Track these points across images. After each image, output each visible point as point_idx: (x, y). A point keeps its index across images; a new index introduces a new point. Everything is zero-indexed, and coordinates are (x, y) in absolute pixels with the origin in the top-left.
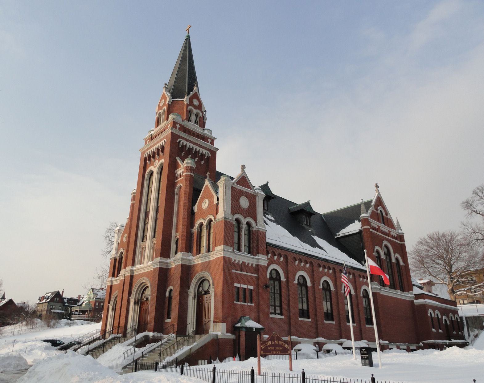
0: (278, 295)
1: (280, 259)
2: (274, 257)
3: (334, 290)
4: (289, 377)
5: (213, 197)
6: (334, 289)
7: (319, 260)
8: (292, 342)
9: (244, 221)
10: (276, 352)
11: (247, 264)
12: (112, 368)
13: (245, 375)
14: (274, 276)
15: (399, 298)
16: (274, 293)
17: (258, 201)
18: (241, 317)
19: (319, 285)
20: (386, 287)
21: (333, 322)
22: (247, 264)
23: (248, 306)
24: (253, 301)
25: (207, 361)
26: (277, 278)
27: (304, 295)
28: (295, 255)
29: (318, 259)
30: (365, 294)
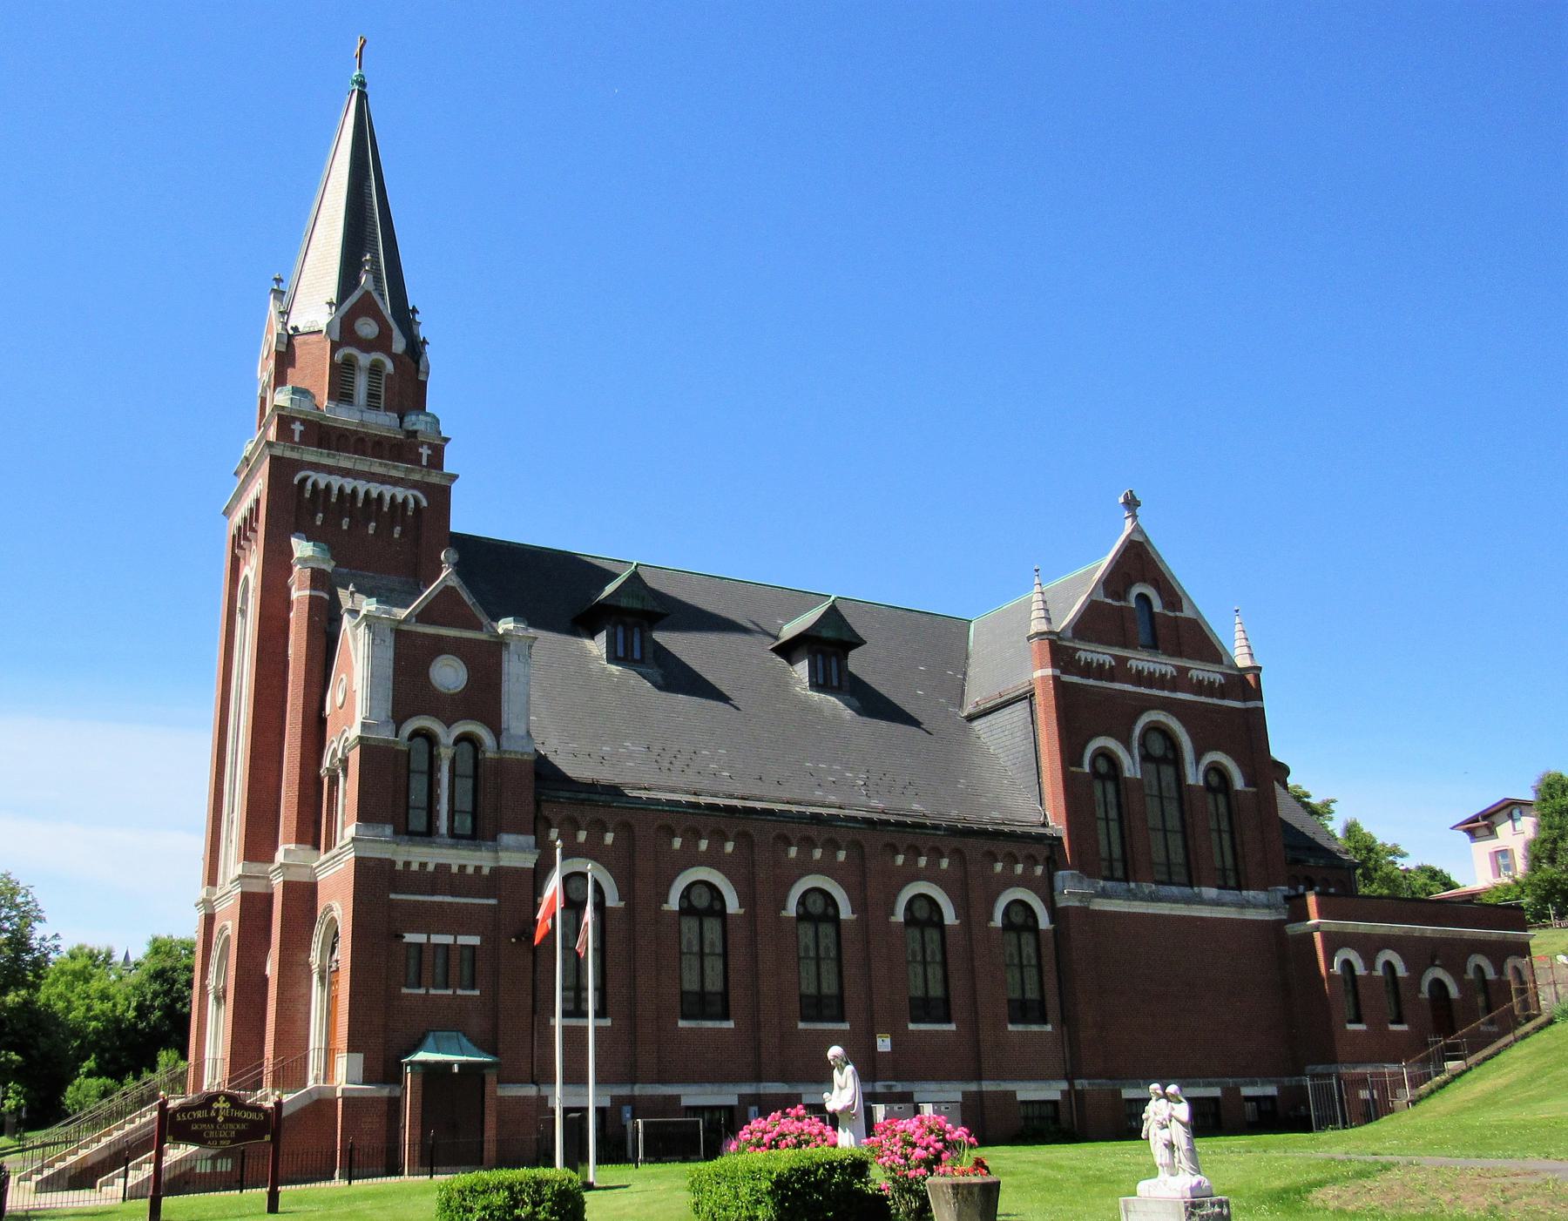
0: (1034, 971)
1: (1013, 870)
2: (919, 859)
6: (620, 899)
7: (781, 821)
8: (1076, 1091)
9: (447, 736)
10: (222, 1133)
11: (455, 869)
12: (187, 1183)
14: (1018, 918)
15: (1255, 918)
16: (1021, 967)
17: (506, 659)
18: (428, 1031)
19: (991, 918)
20: (1135, 881)
22: (455, 869)
25: (230, 1161)
28: (987, 845)
29: (775, 821)
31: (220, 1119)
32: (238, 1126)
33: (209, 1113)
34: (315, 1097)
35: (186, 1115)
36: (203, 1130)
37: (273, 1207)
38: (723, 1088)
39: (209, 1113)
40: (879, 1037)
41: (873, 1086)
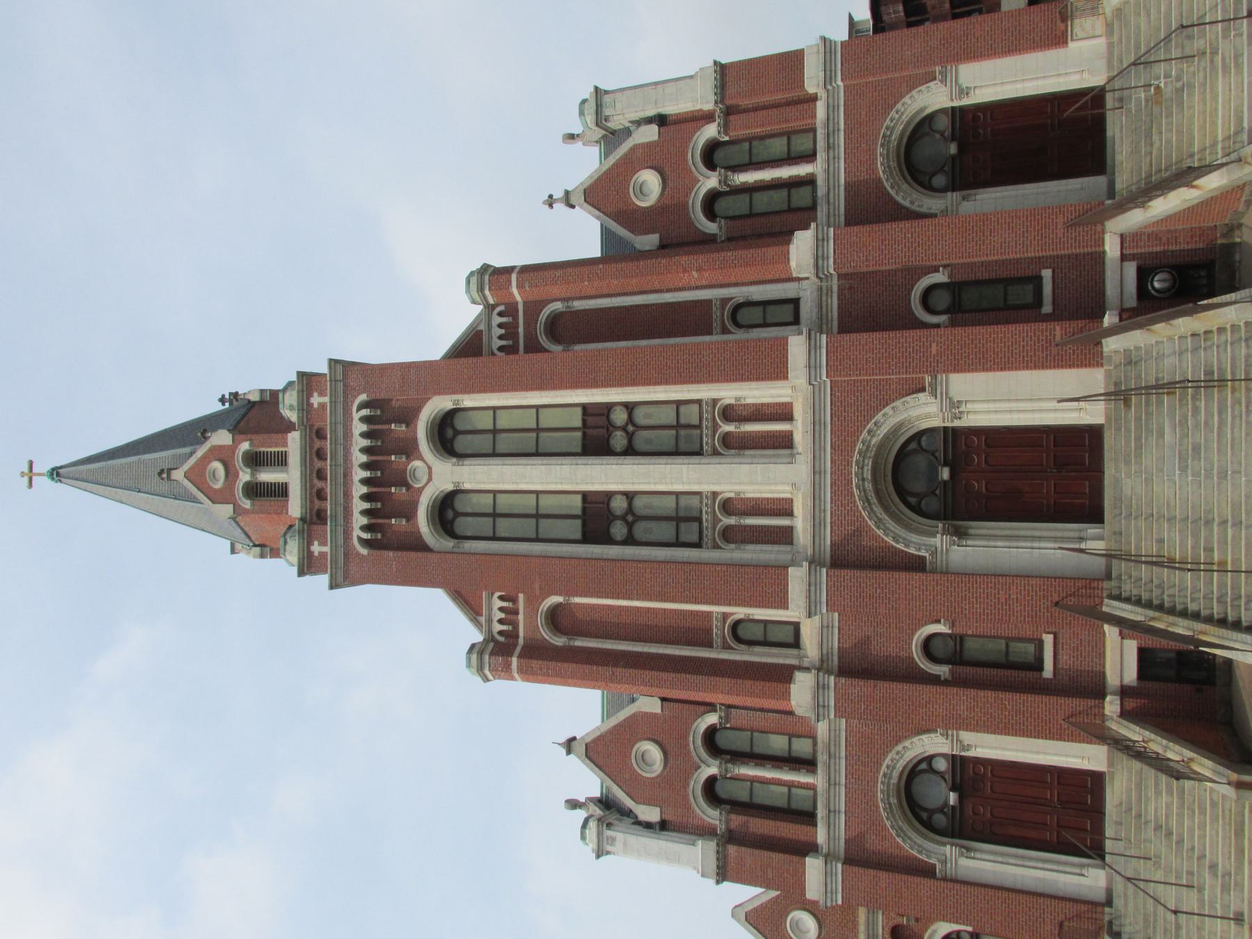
5: (634, 149)
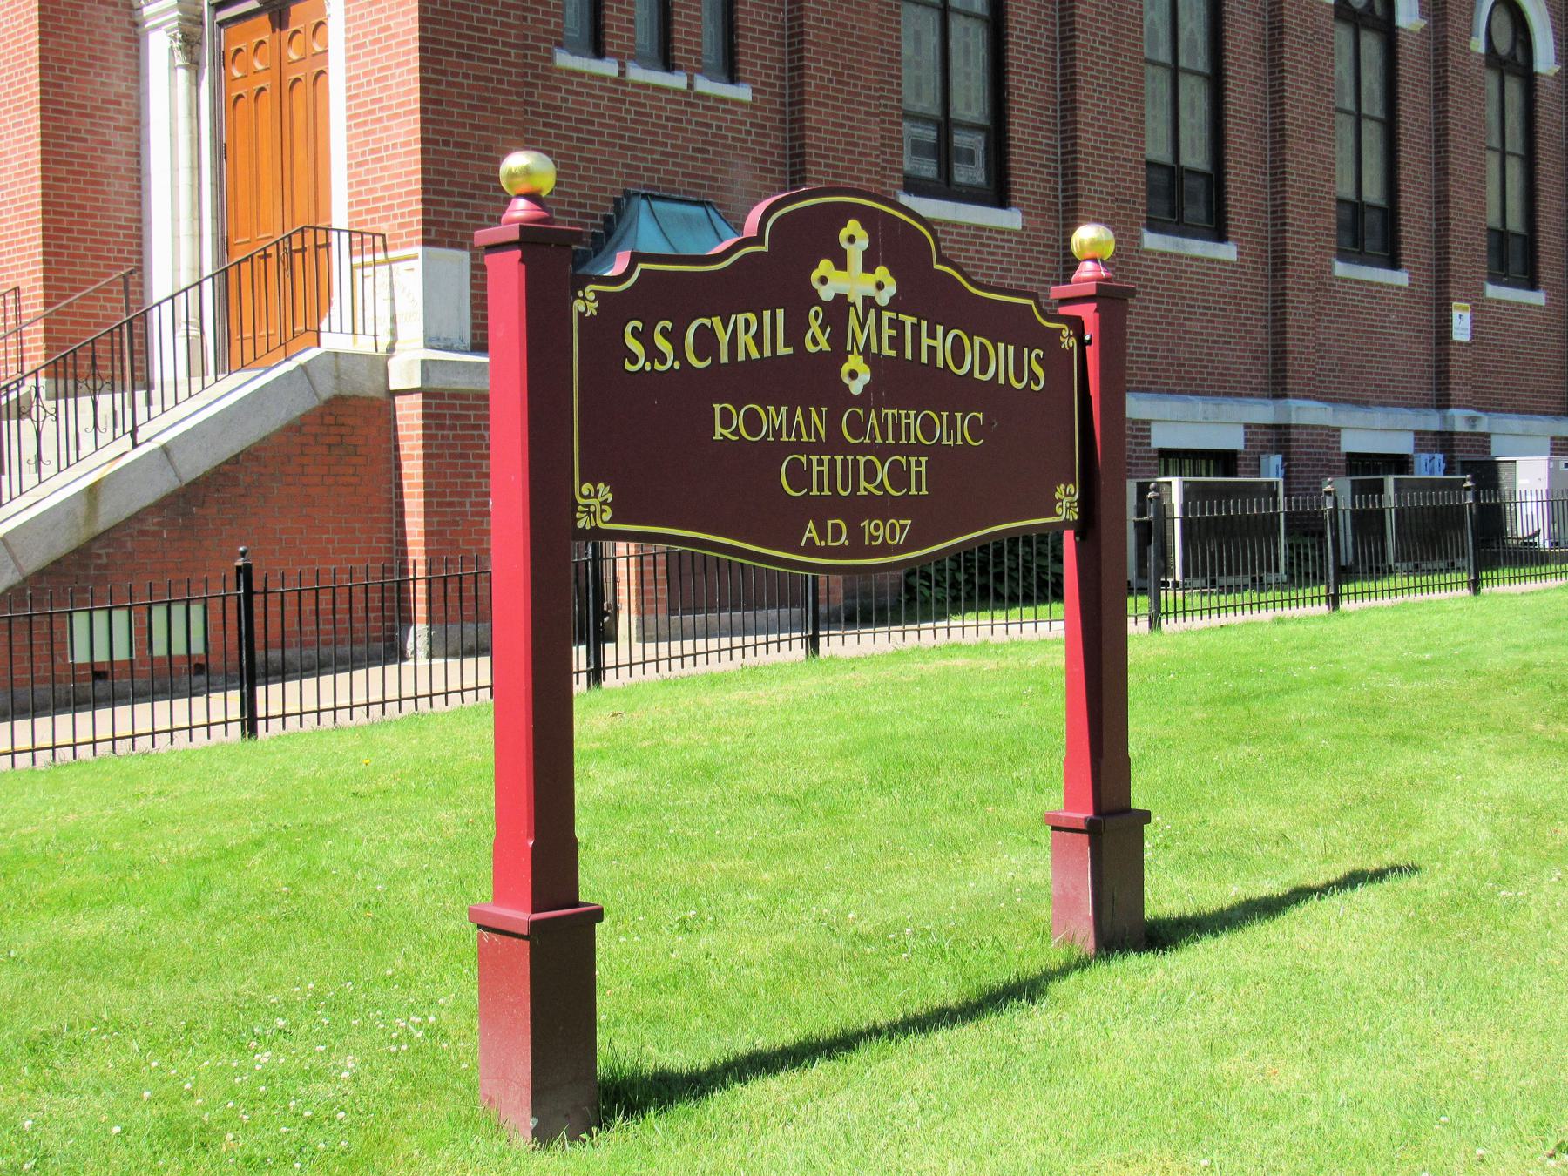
3: (1423, 23)
4: (331, 705)
13: (423, 689)
21: (1222, 246)
23: (691, 98)
24: (744, 57)
26: (1514, 58)
27: (1192, 43)
30: (1503, 44)
31: (857, 375)
32: (940, 429)
33: (796, 331)
34: (327, 389)
35: (676, 338)
36: (774, 451)
37: (250, 724)
38: (1224, 407)
39: (796, 331)
40: (1458, 308)
41: (1444, 418)
